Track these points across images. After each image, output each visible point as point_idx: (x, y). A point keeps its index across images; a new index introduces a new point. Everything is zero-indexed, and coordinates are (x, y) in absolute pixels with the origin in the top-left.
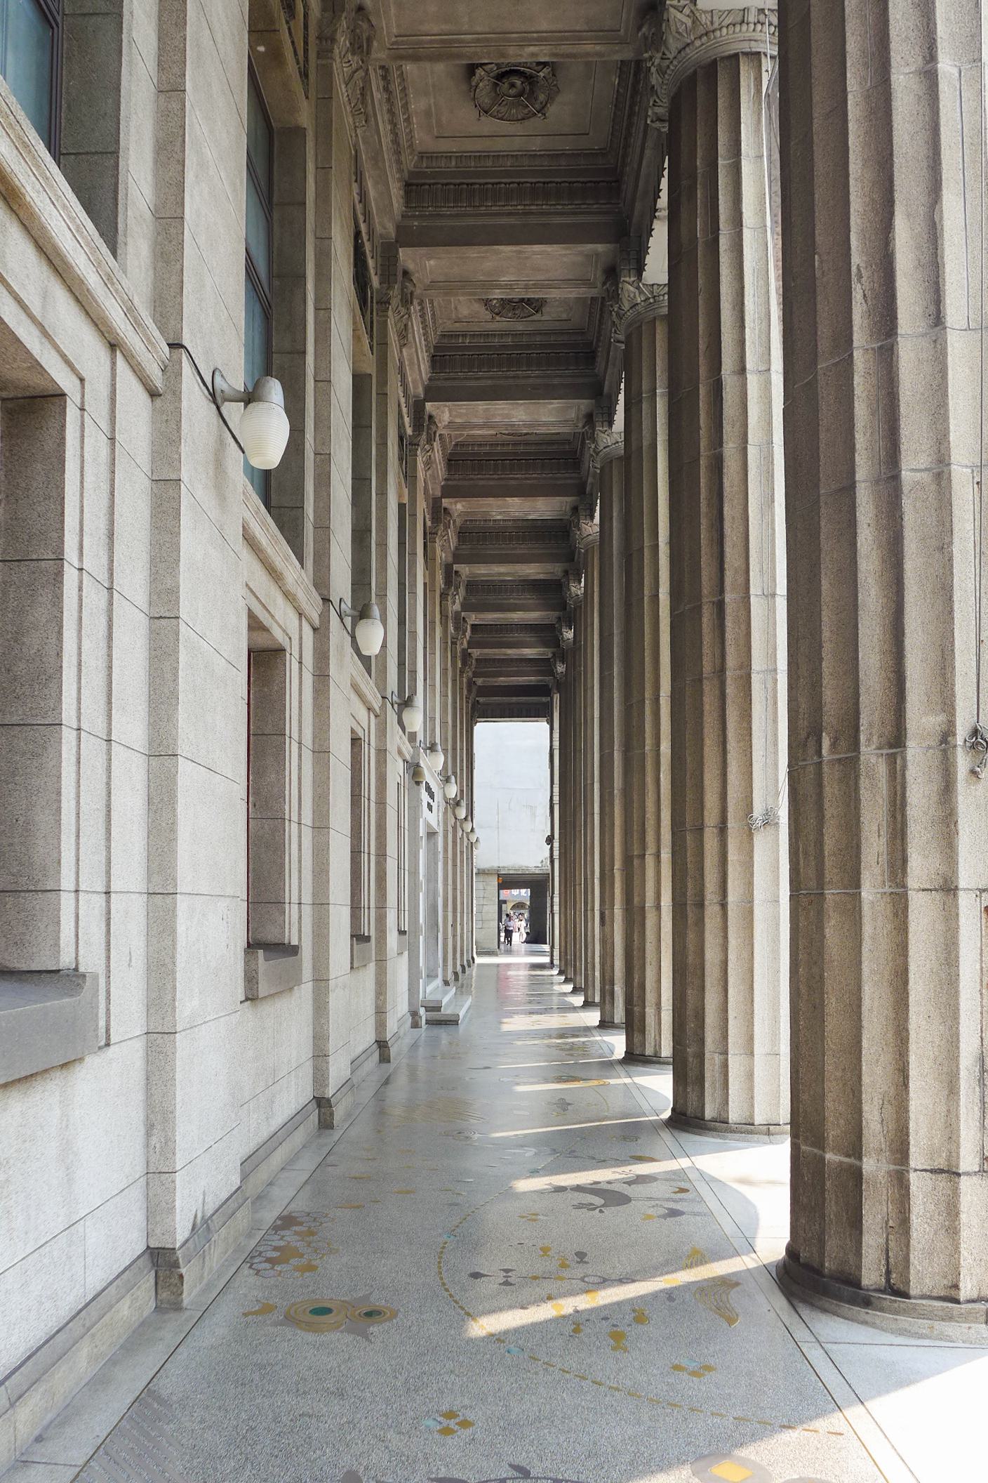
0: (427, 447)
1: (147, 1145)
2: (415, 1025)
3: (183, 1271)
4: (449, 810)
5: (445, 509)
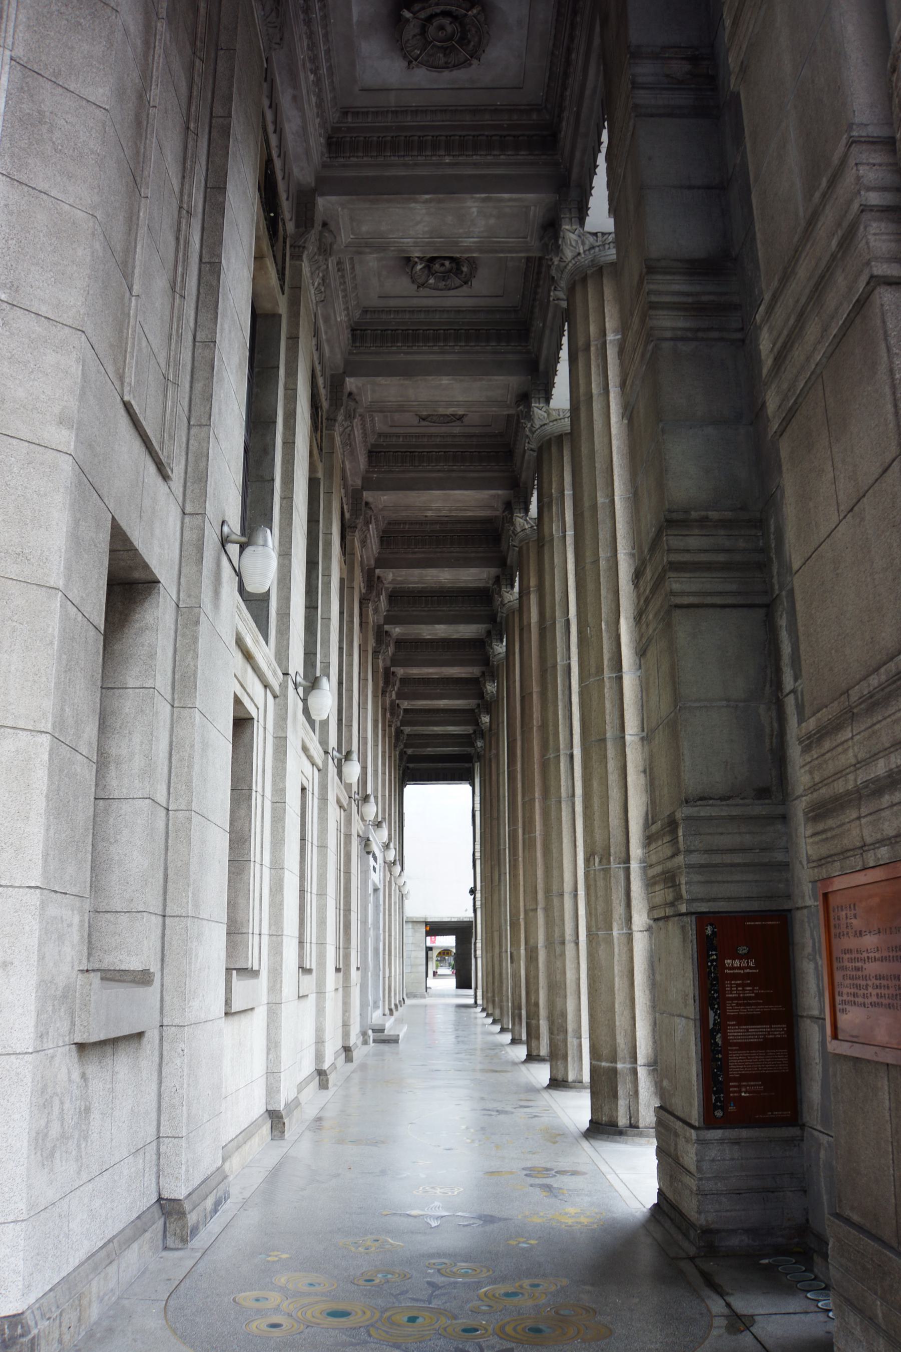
0: (376, 599)
1: (267, 1059)
2: (365, 1042)
3: (285, 1121)
4: (387, 868)
5: (387, 632)
